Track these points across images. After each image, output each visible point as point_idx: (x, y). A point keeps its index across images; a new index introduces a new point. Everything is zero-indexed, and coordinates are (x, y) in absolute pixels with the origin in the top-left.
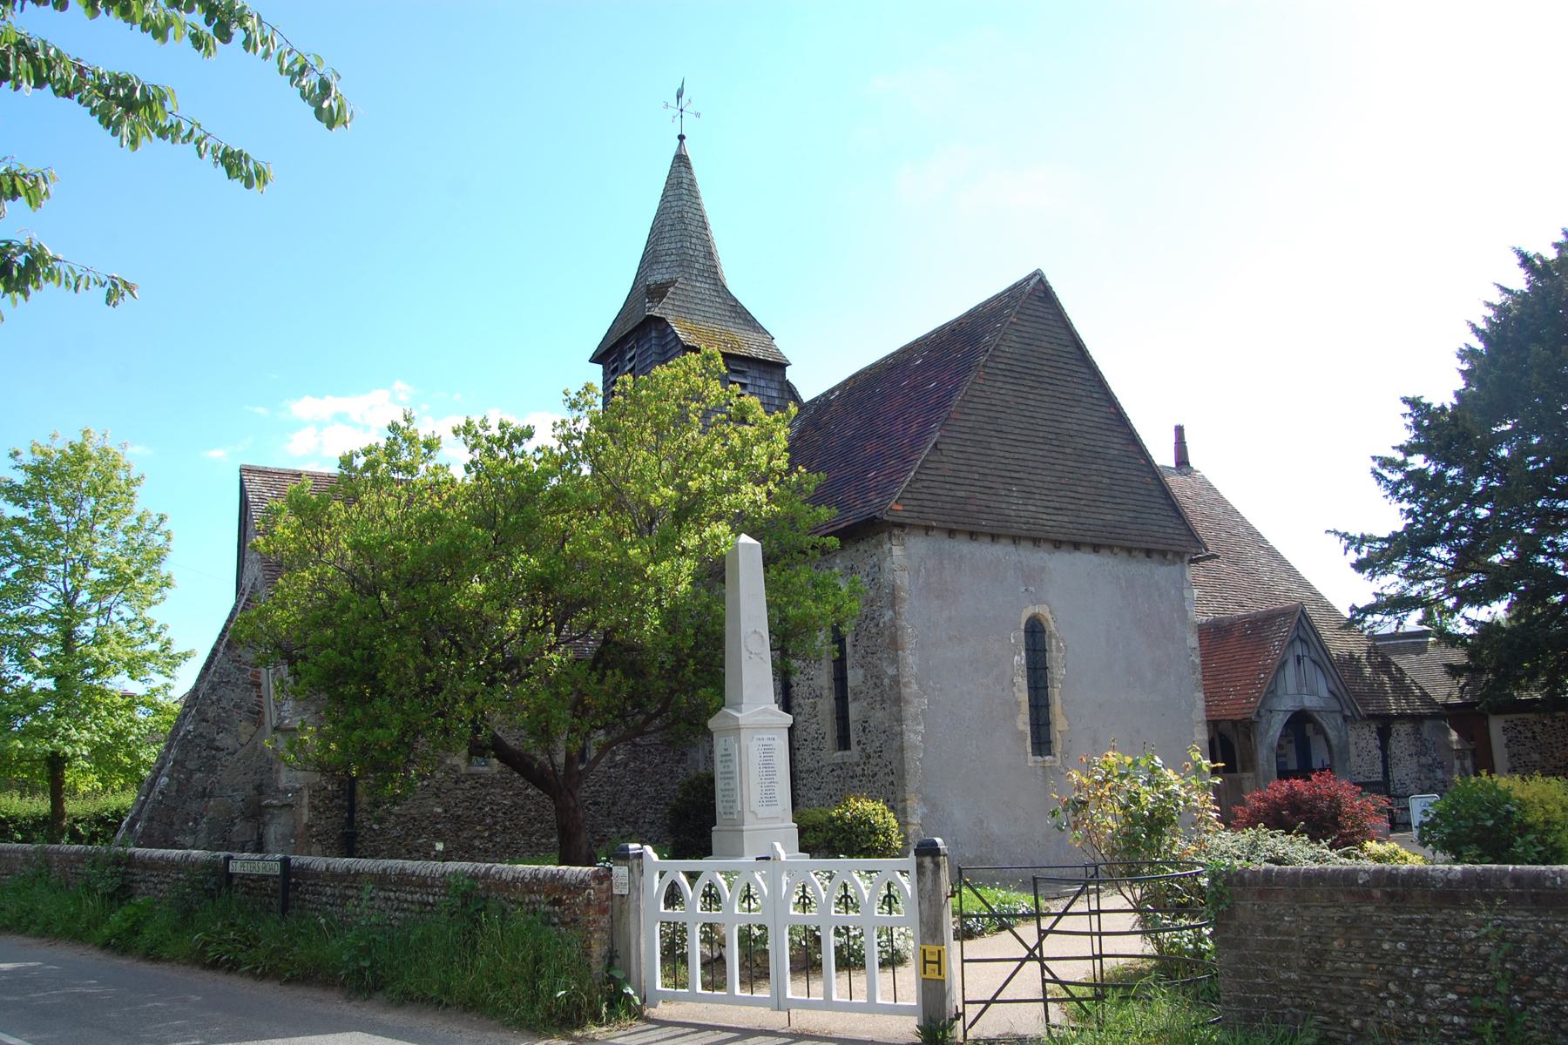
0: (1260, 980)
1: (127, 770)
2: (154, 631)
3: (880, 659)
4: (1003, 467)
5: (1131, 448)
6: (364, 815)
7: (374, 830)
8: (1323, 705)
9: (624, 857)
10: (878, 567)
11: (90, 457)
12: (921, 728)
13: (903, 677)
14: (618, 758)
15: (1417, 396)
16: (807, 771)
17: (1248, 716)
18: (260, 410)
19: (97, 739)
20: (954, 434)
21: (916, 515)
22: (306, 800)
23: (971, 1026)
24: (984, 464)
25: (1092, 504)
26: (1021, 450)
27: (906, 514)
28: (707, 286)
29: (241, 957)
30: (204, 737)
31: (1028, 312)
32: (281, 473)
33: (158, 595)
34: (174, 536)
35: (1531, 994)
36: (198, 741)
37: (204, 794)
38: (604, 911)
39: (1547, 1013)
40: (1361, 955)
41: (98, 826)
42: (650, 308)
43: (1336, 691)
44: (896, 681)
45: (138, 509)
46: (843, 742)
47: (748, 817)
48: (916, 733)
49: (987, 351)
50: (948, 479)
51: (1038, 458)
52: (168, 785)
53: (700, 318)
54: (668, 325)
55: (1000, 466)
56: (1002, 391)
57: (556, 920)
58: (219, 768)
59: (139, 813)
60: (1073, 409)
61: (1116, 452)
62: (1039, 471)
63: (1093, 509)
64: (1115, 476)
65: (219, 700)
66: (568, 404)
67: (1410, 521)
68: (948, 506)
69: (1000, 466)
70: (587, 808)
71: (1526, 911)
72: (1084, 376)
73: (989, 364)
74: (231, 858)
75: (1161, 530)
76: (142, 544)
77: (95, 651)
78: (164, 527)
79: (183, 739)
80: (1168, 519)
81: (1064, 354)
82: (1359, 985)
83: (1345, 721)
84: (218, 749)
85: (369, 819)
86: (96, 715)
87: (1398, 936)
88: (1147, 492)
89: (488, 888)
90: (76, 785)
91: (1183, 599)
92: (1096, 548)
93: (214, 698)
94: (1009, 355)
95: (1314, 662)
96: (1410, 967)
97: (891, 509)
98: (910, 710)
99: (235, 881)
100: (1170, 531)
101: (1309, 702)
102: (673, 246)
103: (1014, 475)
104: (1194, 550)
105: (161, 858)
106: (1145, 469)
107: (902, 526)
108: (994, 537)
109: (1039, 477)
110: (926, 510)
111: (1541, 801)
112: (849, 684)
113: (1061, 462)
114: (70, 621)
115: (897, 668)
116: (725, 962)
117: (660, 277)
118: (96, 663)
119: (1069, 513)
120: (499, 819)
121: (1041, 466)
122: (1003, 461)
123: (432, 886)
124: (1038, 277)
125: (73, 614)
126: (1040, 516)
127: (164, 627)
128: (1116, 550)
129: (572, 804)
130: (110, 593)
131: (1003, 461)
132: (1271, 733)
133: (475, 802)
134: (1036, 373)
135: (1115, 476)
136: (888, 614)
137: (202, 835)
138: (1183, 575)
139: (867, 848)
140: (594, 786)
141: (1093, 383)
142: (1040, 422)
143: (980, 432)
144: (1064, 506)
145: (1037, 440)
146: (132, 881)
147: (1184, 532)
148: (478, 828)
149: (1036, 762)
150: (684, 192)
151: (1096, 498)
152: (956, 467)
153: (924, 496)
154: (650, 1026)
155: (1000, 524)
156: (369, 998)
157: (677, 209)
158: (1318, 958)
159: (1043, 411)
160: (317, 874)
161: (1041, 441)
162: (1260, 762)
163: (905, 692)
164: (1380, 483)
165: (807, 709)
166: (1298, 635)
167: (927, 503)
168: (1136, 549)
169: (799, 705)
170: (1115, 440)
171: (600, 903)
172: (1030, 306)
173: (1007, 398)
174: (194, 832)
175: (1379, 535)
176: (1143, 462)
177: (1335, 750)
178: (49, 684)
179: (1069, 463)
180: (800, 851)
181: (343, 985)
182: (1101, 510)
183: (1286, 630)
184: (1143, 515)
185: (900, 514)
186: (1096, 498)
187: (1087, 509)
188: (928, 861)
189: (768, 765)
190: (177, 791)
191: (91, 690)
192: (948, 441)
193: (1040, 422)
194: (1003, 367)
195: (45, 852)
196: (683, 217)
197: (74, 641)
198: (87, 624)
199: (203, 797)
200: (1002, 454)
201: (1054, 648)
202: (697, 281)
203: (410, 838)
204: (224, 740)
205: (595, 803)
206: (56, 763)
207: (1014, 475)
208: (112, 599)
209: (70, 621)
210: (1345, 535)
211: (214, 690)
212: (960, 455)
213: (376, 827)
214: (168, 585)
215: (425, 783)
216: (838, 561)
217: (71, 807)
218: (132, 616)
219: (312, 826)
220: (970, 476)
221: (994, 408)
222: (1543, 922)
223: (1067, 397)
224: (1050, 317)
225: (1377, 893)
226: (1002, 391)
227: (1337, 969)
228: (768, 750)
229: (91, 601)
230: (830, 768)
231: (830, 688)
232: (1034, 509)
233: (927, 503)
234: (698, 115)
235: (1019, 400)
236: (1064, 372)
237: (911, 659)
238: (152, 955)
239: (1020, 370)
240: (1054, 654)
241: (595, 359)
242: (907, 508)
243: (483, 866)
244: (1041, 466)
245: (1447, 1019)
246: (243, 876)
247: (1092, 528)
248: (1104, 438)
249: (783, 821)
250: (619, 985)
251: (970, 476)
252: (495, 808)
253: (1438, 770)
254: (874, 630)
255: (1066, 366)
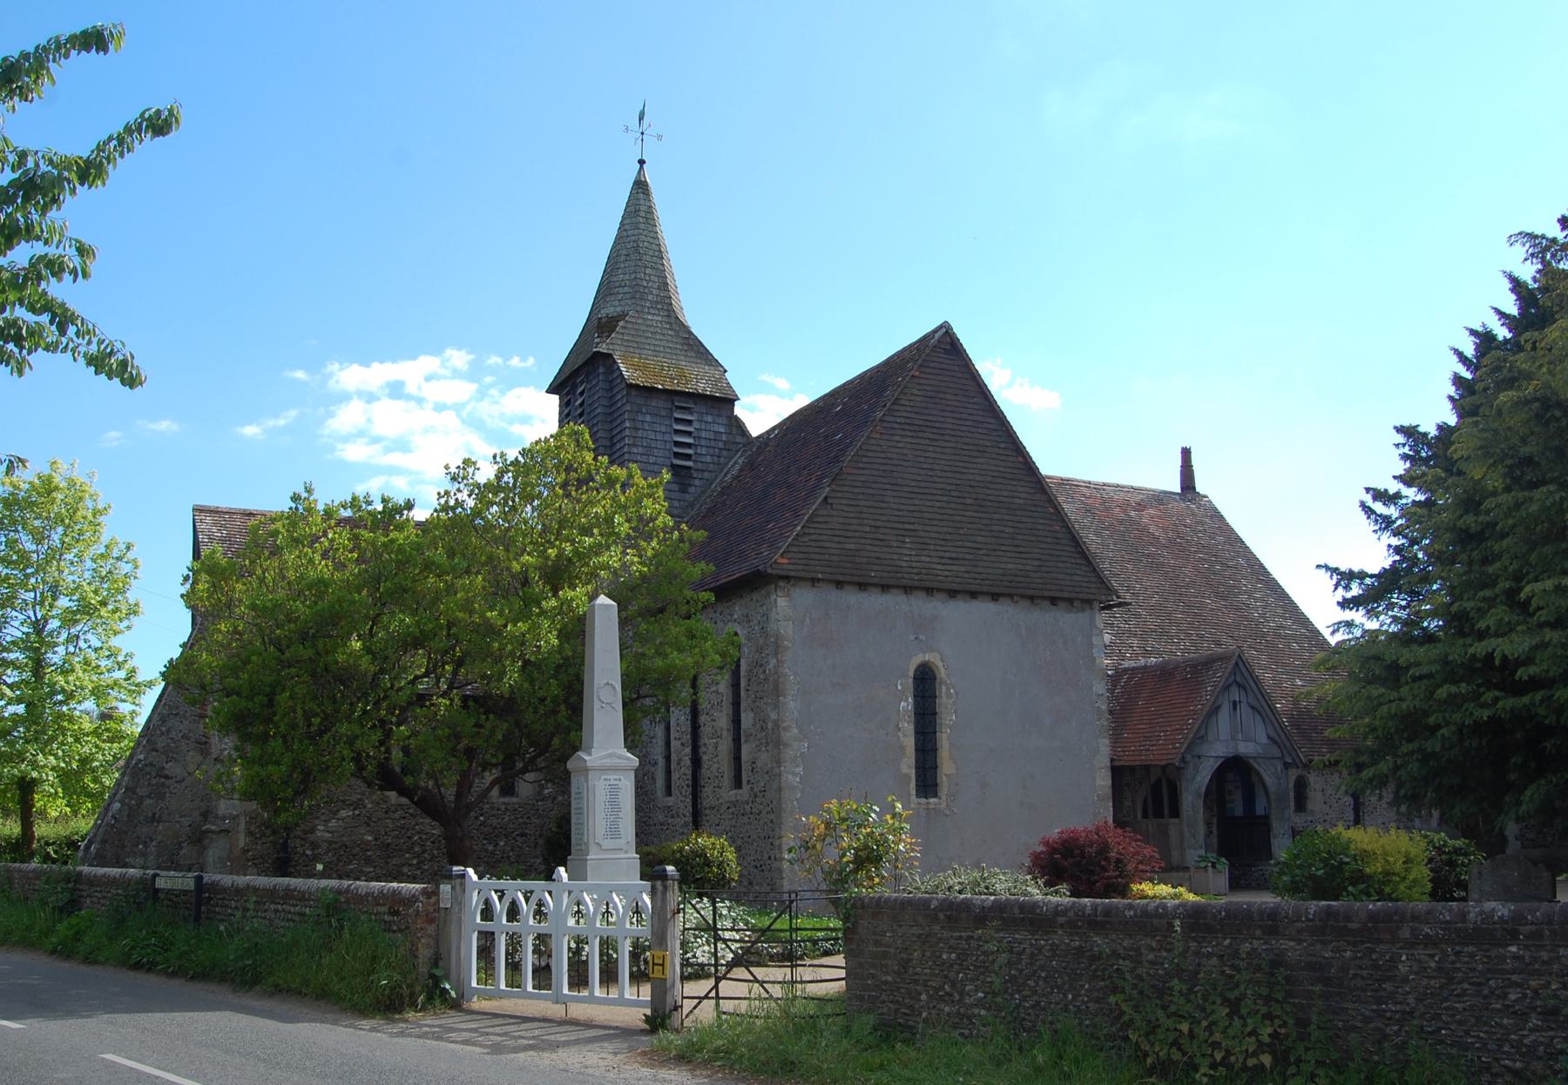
0: (869, 982)
1: (94, 795)
2: (120, 659)
3: (766, 704)
4: (896, 519)
5: (1038, 497)
6: (298, 841)
7: (307, 856)
8: (1260, 751)
9: (449, 877)
10: (766, 616)
11: (57, 488)
12: (800, 770)
13: (784, 721)
14: (546, 791)
15: (1414, 424)
16: (710, 808)
17: (1171, 762)
18: (300, 374)
19: (63, 765)
20: (846, 489)
21: (801, 567)
22: (242, 826)
23: (687, 1016)
24: (877, 517)
25: (992, 553)
26: (917, 502)
27: (791, 567)
28: (659, 318)
29: (159, 959)
30: (154, 766)
31: (932, 365)
32: (230, 513)
33: (126, 623)
34: (141, 562)
35: (1024, 993)
36: (148, 769)
37: (154, 819)
38: (431, 921)
39: (1033, 1007)
40: (930, 963)
41: (69, 849)
42: (598, 343)
43: (1277, 738)
44: (776, 723)
45: (105, 538)
46: (738, 782)
47: (592, 848)
48: (795, 774)
49: (885, 405)
50: (837, 533)
51: (936, 510)
52: (120, 810)
53: (650, 353)
54: (615, 362)
55: (892, 518)
56: (899, 445)
57: (395, 928)
58: (168, 795)
59: (94, 836)
60: (977, 460)
61: (1022, 501)
62: (935, 523)
63: (993, 559)
64: (1019, 525)
65: (168, 731)
66: (449, 477)
67: (1397, 558)
68: (836, 558)
69: (892, 518)
70: (514, 838)
71: (1027, 931)
72: (991, 426)
73: (887, 418)
74: (158, 875)
75: (1068, 578)
76: (110, 572)
77: (61, 680)
78: (130, 556)
79: (134, 767)
80: (1078, 567)
81: (970, 406)
82: (927, 986)
83: (1287, 768)
84: (166, 777)
85: (302, 845)
86: (62, 741)
87: (952, 949)
88: (1055, 541)
89: (348, 901)
90: (45, 809)
91: (1091, 645)
92: (995, 597)
93: (164, 729)
94: (909, 409)
95: (1253, 707)
96: (958, 974)
97: (775, 562)
98: (789, 753)
99: (162, 896)
100: (1077, 578)
101: (1245, 748)
102: (627, 277)
103: (907, 526)
104: (1103, 598)
105: (104, 876)
106: (1054, 518)
107: (787, 578)
108: (885, 588)
109: (935, 529)
110: (812, 562)
111: (1385, 854)
112: (742, 727)
113: (961, 513)
114: (39, 649)
115: (778, 713)
116: (551, 971)
117: (612, 309)
118: (63, 691)
119: (966, 562)
120: (428, 848)
121: (938, 517)
122: (898, 513)
123: (309, 900)
124: (944, 330)
125: (42, 642)
126: (934, 566)
127: (129, 656)
128: (1016, 598)
129: (460, 834)
130: (76, 622)
131: (898, 513)
132: (1199, 779)
133: (403, 831)
134: (937, 425)
135: (1019, 525)
136: (773, 661)
137: (151, 857)
138: (1092, 622)
139: (701, 878)
140: (522, 817)
141: (1001, 433)
142: (939, 474)
143: (874, 486)
144: (961, 556)
145: (934, 492)
146: (80, 897)
147: (1093, 579)
148: (407, 855)
149: (919, 804)
150: (641, 220)
151: (997, 547)
152: (847, 521)
153: (811, 549)
154: (469, 1017)
155: (891, 575)
156: (250, 990)
157: (633, 238)
158: (905, 964)
159: (943, 462)
160: (224, 890)
161: (939, 492)
162: (1185, 807)
163: (786, 736)
164: (1368, 518)
165: (711, 749)
166: (1235, 680)
167: (813, 556)
168: (1039, 597)
169: (705, 744)
170: (1021, 489)
171: (427, 915)
172: (935, 359)
173: (905, 451)
174: (144, 855)
175: (1370, 572)
176: (1052, 511)
177: (1273, 797)
178: (20, 709)
179: (968, 514)
180: (641, 879)
181: (233, 980)
182: (1004, 559)
183: (1219, 675)
184: (1048, 564)
185: (785, 567)
186: (997, 547)
187: (985, 558)
188: (659, 884)
189: (614, 803)
190: (128, 815)
191: (60, 716)
192: (839, 495)
193: (939, 474)
194: (903, 420)
195: (7, 870)
196: (638, 246)
197: (43, 668)
198: (55, 653)
199: (152, 822)
200: (896, 507)
201: (944, 695)
202: (649, 313)
203: (341, 864)
204: (172, 769)
205: (522, 835)
206: (26, 788)
207: (907, 526)
208: (79, 628)
209: (39, 649)
210: (1335, 570)
211: (164, 721)
212: (852, 509)
213: (309, 852)
214: (135, 613)
215: (357, 812)
216: (737, 608)
217: (41, 830)
218: (99, 644)
219: (248, 851)
220: (860, 528)
221: (890, 462)
222: (1036, 940)
223: (971, 448)
224: (956, 368)
225: (941, 916)
226: (899, 445)
227: (916, 974)
228: (614, 791)
229: (60, 627)
230: (727, 805)
231: (728, 730)
232: (928, 559)
233: (813, 556)
234: (660, 137)
235: (918, 453)
236: (968, 423)
237: (792, 704)
238: (89, 960)
239: (921, 423)
240: (944, 699)
241: (551, 390)
242: (792, 561)
243: (346, 883)
244: (938, 517)
245: (976, 1011)
246: (169, 891)
247: (990, 577)
248: (1009, 488)
249: (626, 852)
250: (436, 981)
251: (860, 528)
252: (424, 837)
253: (1416, 820)
254: (762, 676)
255: (971, 418)
